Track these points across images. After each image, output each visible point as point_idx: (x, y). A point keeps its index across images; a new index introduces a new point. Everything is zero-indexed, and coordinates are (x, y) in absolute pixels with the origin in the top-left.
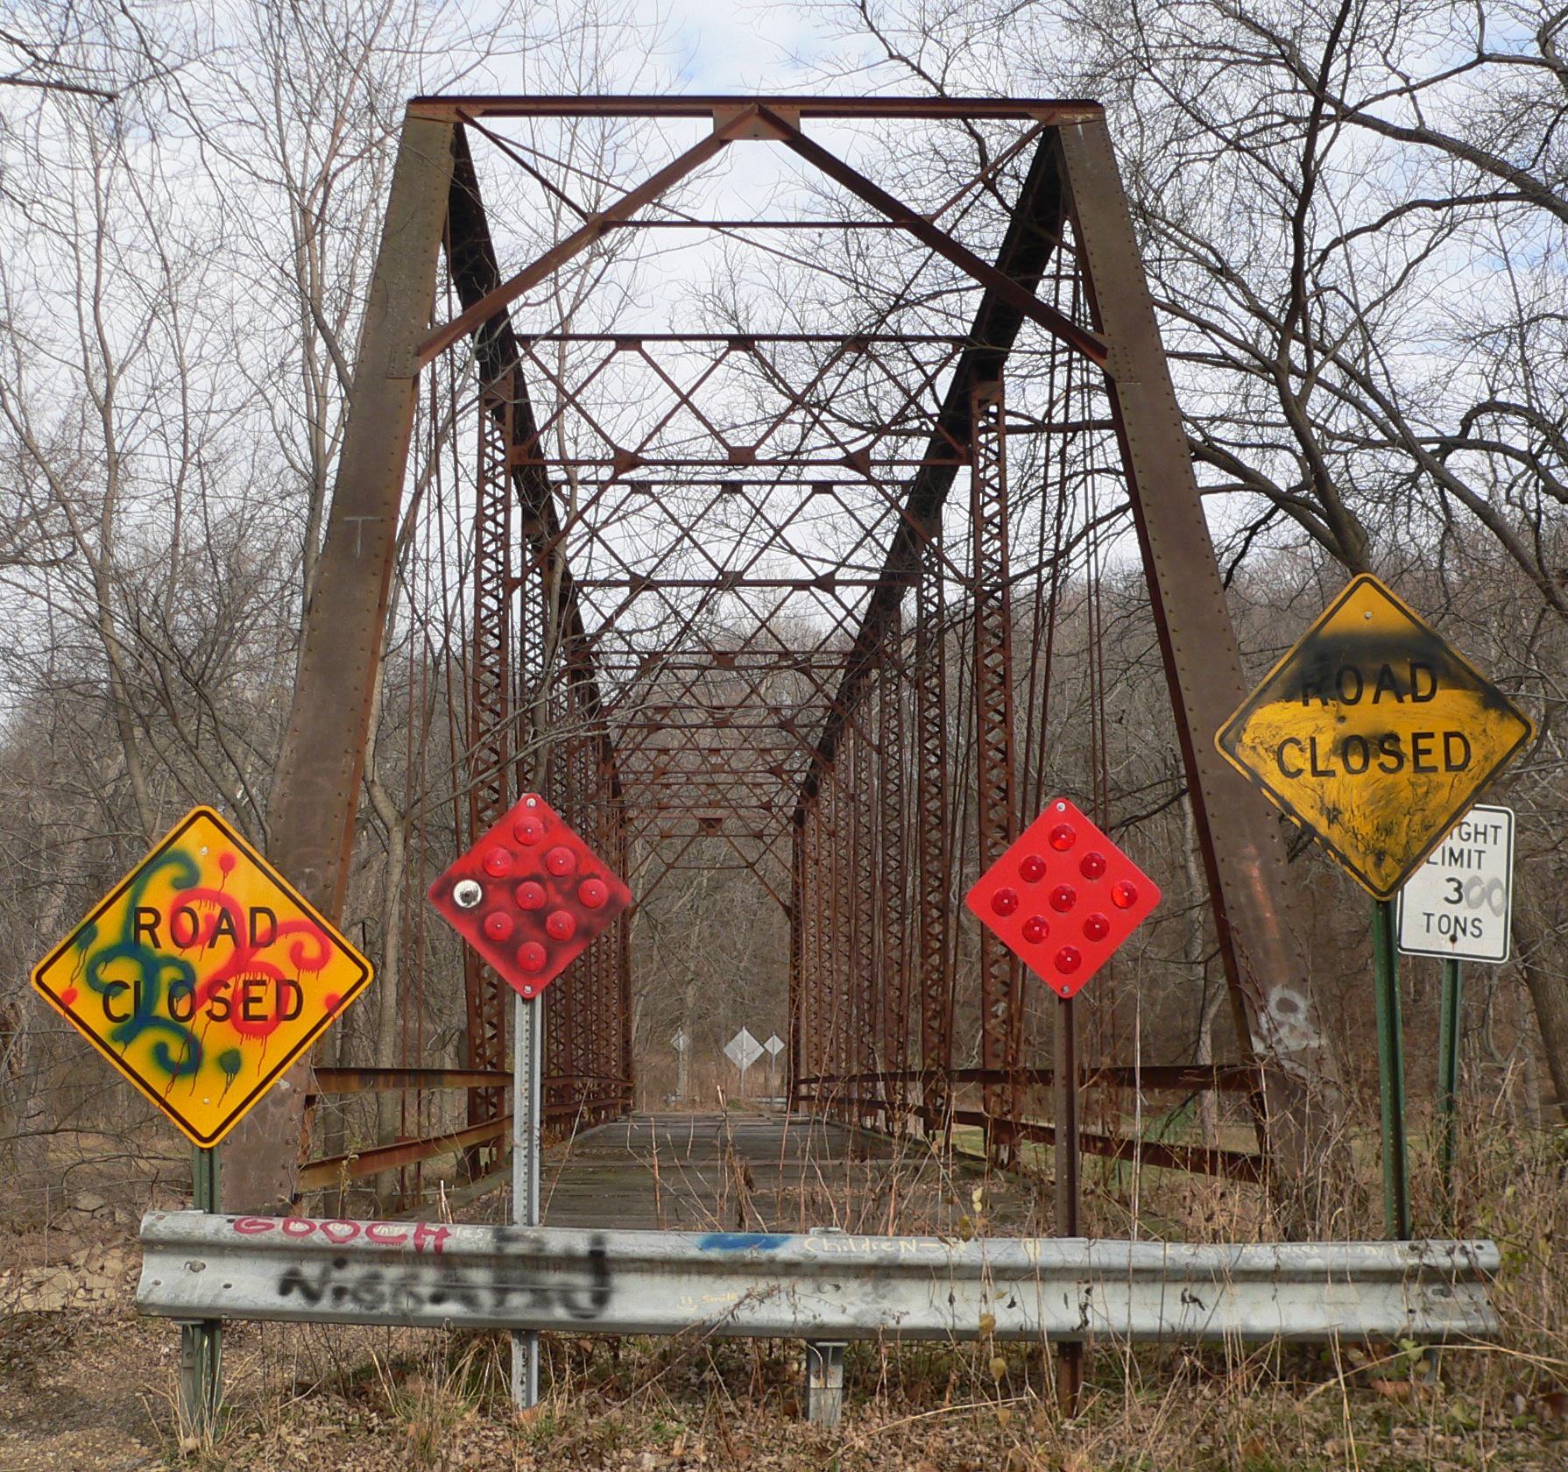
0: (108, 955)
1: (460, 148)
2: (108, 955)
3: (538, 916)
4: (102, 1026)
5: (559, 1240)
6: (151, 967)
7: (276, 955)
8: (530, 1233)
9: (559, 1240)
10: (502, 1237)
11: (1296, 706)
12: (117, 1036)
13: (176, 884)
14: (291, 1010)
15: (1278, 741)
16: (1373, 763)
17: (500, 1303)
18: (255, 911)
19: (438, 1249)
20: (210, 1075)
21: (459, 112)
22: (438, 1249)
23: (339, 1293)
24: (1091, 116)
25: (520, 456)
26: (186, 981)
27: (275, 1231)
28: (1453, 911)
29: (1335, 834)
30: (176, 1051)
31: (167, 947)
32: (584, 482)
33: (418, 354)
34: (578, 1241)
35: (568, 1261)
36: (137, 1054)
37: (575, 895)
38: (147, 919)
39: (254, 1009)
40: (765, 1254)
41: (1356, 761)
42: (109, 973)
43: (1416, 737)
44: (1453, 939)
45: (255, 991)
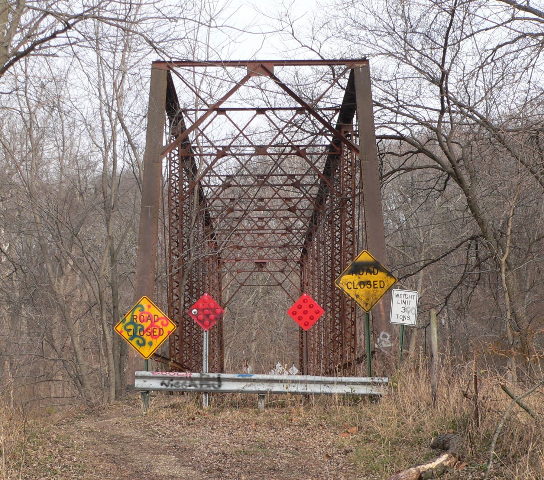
0: (128, 324)
1: (169, 75)
2: (128, 324)
3: (208, 316)
4: (127, 337)
5: (212, 375)
6: (136, 326)
7: (159, 324)
8: (207, 374)
9: (212, 375)
10: (202, 375)
11: (351, 276)
12: (130, 339)
13: (140, 311)
14: (161, 334)
15: (347, 283)
16: (365, 286)
17: (201, 387)
18: (155, 315)
19: (190, 377)
20: (147, 346)
21: (169, 67)
22: (190, 377)
23: (172, 385)
24: (365, 64)
25: (184, 153)
26: (142, 329)
27: (160, 374)
28: (403, 314)
29: (358, 300)
30: (141, 342)
31: (139, 322)
32: (201, 110)
33: (162, 154)
34: (216, 375)
35: (213, 379)
36: (134, 342)
37: (215, 312)
38: (135, 317)
39: (155, 334)
40: (249, 378)
41: (362, 286)
42: (128, 327)
43: (374, 282)
44: (403, 320)
45: (155, 330)
